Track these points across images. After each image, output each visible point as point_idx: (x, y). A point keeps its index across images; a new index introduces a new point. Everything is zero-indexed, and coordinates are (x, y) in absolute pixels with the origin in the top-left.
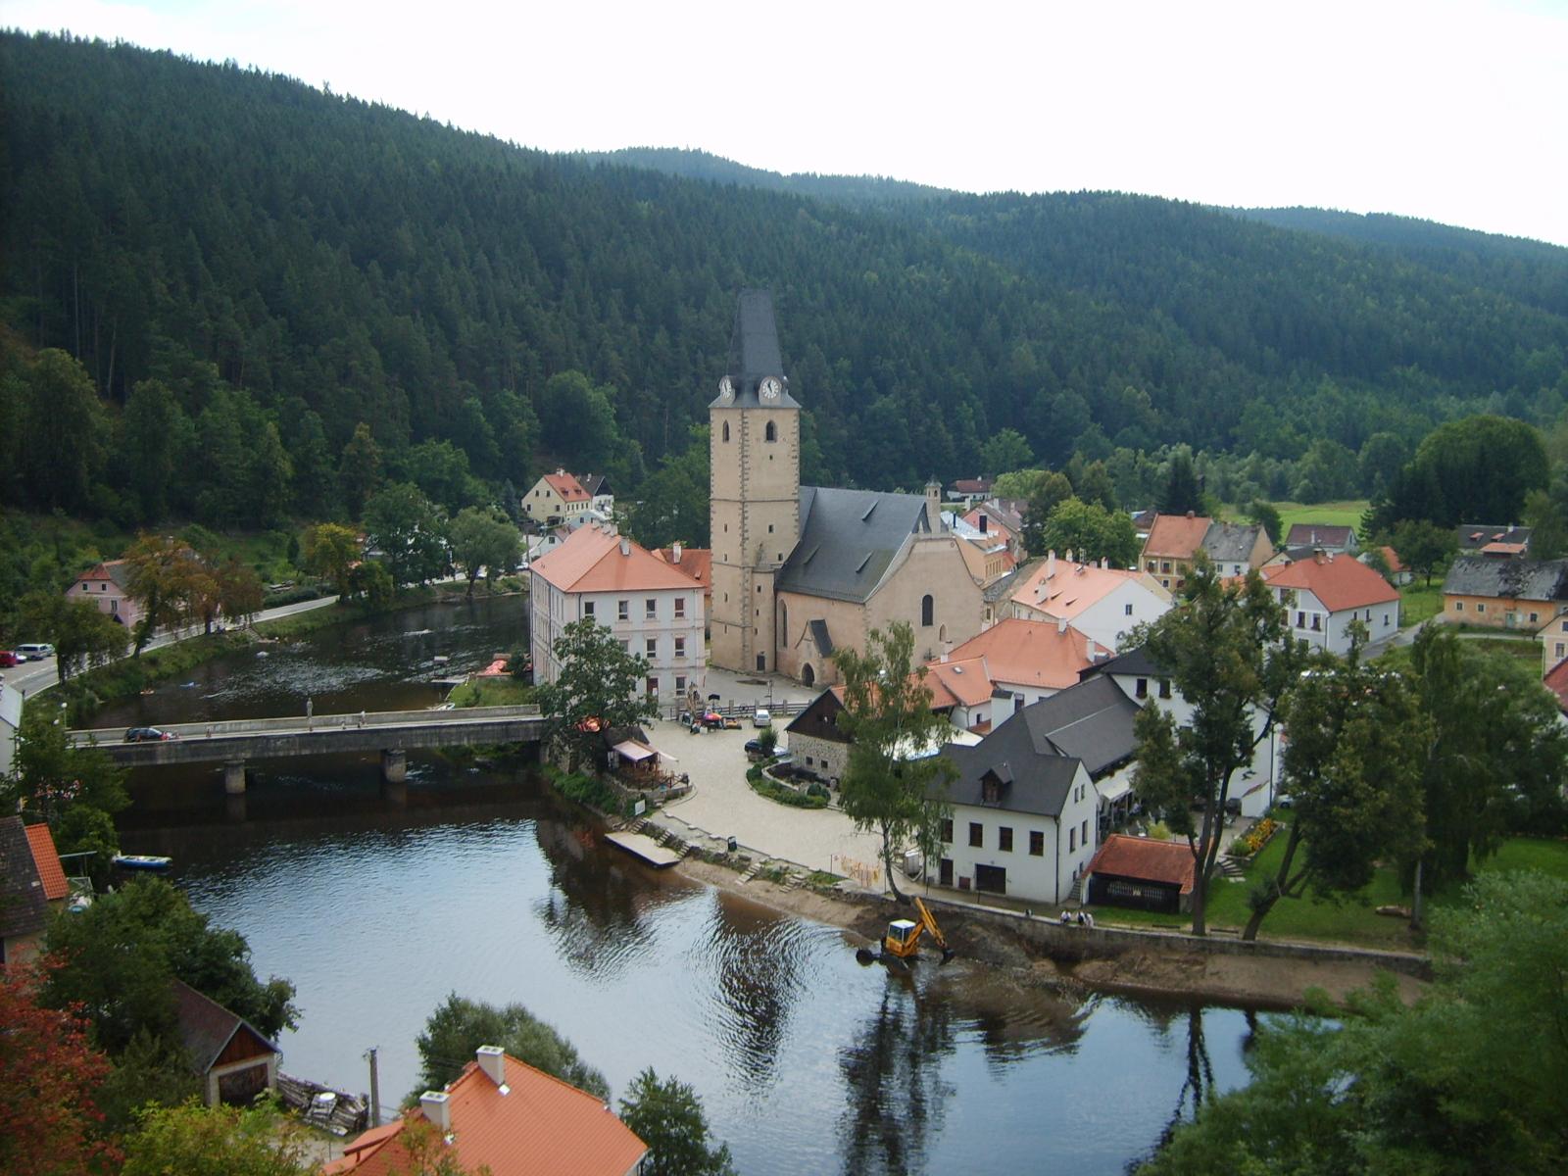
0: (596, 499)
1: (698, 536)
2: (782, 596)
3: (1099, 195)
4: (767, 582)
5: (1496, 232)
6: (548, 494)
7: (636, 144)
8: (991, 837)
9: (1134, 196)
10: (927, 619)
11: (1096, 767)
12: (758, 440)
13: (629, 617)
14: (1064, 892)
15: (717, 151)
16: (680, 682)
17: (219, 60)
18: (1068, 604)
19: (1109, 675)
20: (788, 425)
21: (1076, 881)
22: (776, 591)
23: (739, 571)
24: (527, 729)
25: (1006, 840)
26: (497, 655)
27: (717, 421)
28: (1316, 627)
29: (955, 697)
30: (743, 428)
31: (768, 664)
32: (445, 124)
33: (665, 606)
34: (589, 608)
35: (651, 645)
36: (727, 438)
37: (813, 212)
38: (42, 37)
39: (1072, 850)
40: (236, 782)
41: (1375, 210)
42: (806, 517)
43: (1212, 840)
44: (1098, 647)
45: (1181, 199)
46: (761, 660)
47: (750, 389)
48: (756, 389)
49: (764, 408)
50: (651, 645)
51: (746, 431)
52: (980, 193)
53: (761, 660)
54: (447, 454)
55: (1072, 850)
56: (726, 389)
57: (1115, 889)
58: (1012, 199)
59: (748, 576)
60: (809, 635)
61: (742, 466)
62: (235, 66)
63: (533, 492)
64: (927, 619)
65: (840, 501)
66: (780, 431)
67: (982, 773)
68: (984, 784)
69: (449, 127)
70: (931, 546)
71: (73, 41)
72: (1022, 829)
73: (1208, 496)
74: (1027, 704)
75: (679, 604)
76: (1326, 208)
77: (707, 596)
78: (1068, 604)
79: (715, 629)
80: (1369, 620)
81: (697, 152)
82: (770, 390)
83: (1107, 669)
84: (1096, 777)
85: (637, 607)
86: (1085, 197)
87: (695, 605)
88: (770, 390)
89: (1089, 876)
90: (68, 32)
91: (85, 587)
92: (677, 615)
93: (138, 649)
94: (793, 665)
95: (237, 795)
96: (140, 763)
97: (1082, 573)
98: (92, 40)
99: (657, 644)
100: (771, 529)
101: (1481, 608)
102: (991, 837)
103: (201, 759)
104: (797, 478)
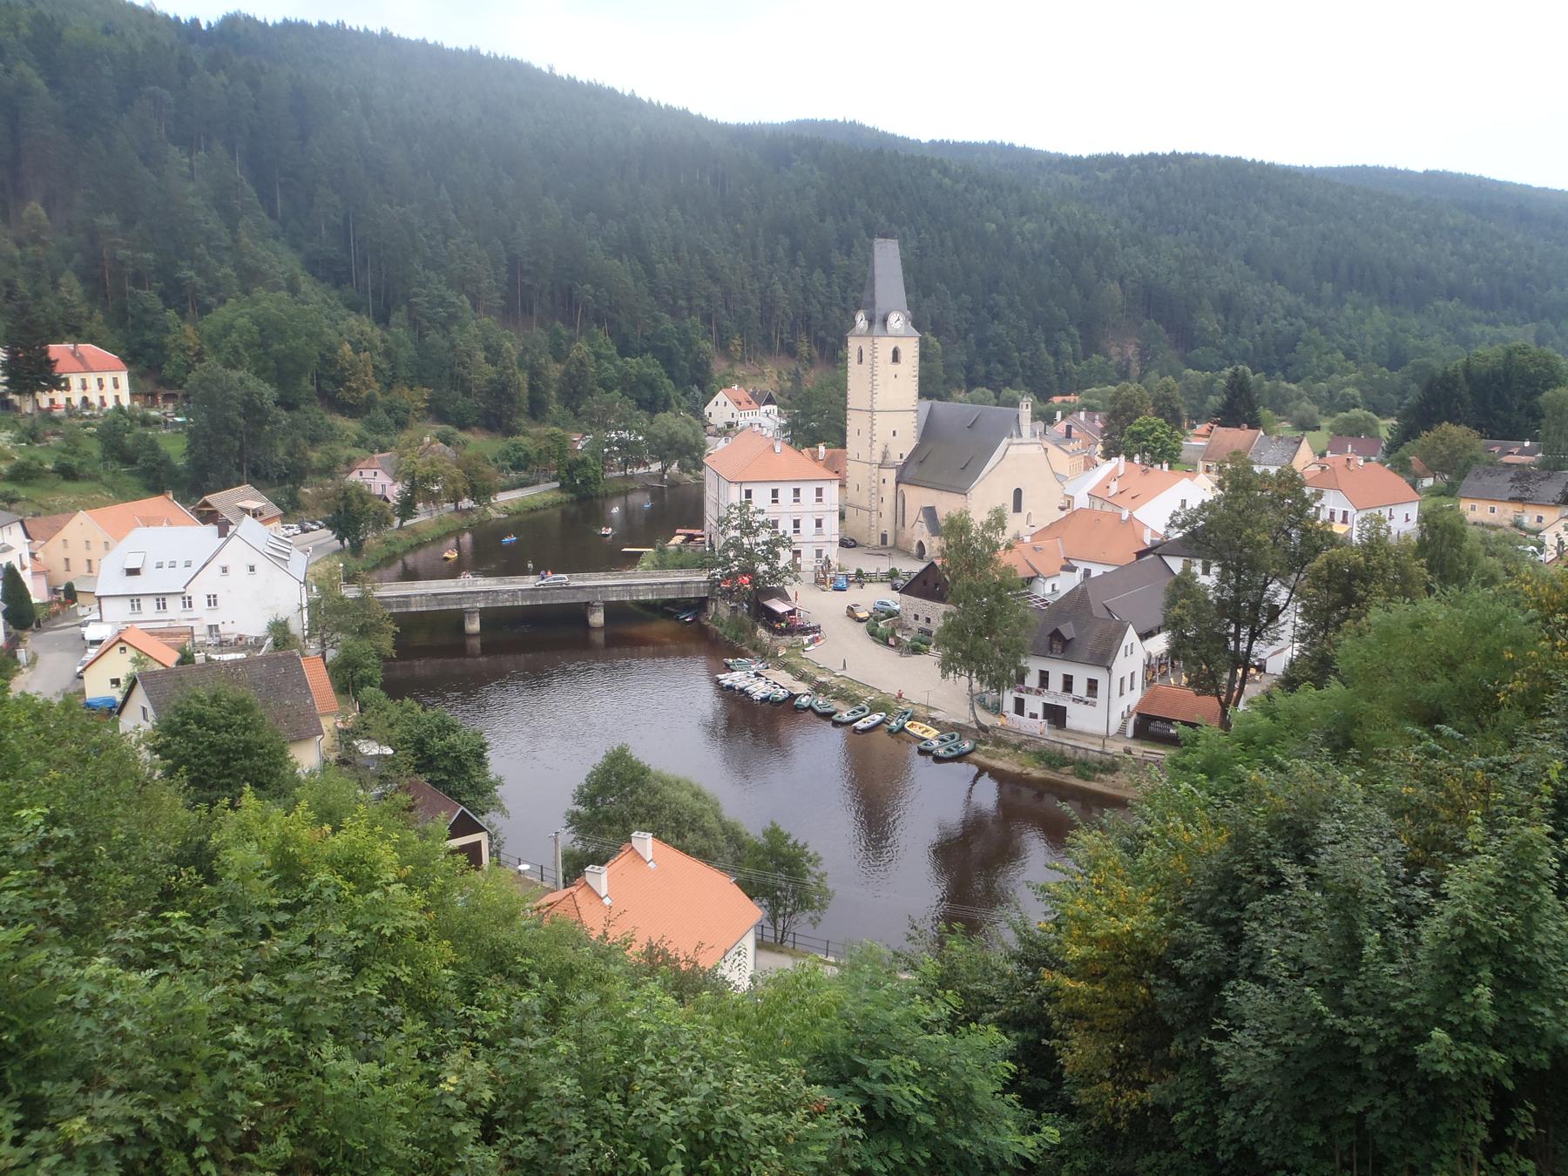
0: (764, 408)
1: (836, 434)
2: (902, 486)
3: (1189, 156)
4: (891, 475)
5: (1542, 185)
7: (802, 117)
8: (1056, 683)
9: (1217, 157)
10: (1017, 507)
11: (1145, 630)
12: (885, 361)
14: (1114, 729)
15: (869, 122)
16: (819, 553)
17: (465, 47)
19: (1160, 555)
20: (910, 349)
21: (1125, 719)
22: (897, 483)
24: (698, 588)
25: (1068, 683)
26: (678, 531)
27: (853, 344)
28: (1345, 521)
29: (1035, 570)
31: (890, 542)
33: (808, 492)
34: (748, 494)
35: (796, 524)
37: (945, 171)
38: (323, 27)
39: (1121, 694)
40: (474, 626)
41: (1432, 167)
42: (925, 418)
43: (1235, 694)
44: (1154, 533)
45: (1258, 160)
46: (884, 537)
47: (878, 322)
48: (885, 321)
50: (796, 524)
53: (884, 537)
54: (645, 366)
55: (1121, 694)
56: (861, 320)
57: (1155, 727)
58: (1112, 161)
59: (875, 470)
60: (921, 518)
62: (478, 51)
63: (713, 402)
64: (1017, 507)
65: (959, 408)
66: (903, 356)
67: (1050, 631)
68: (1051, 641)
72: (1081, 675)
73: (1265, 413)
74: (1093, 575)
75: (819, 492)
77: (842, 486)
79: (849, 512)
80: (1391, 518)
81: (853, 123)
83: (1158, 551)
84: (1144, 636)
85: (786, 493)
86: (1175, 157)
87: (832, 491)
88: (897, 321)
89: (1135, 716)
91: (361, 474)
92: (817, 500)
93: (401, 523)
94: (909, 542)
95: (474, 635)
96: (399, 610)
97: (1145, 472)
99: (801, 523)
101: (1493, 510)
102: (1056, 683)
103: (445, 608)
104: (916, 393)
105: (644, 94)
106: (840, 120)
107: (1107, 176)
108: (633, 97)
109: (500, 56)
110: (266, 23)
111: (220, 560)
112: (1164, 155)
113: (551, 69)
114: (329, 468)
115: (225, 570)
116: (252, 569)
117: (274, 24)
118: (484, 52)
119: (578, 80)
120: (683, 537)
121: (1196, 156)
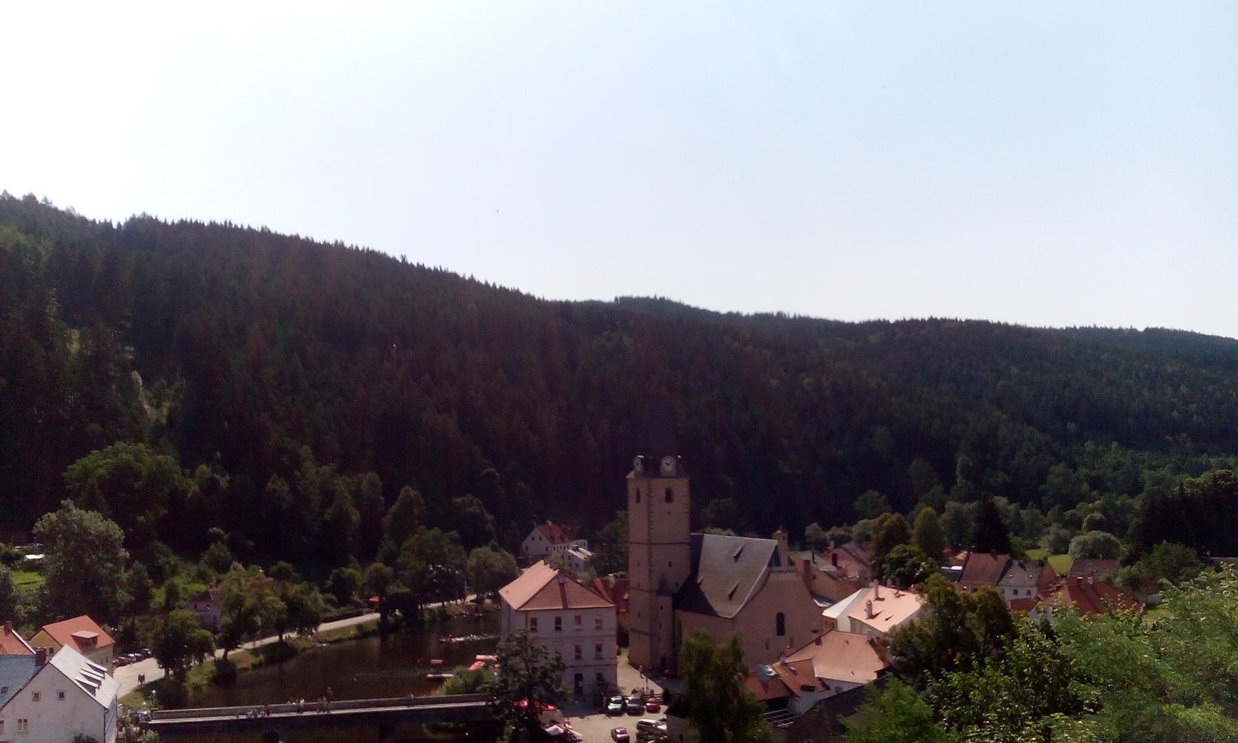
2: (679, 612)
3: (944, 321)
4: (666, 601)
6: (540, 539)
13: (563, 629)
18: (887, 619)
20: (681, 488)
23: (647, 595)
26: (479, 657)
30: (649, 492)
32: (461, 276)
36: (638, 500)
41: (1152, 326)
49: (664, 477)
51: (651, 494)
52: (857, 322)
61: (649, 520)
62: (342, 244)
69: (884, 320)
70: (783, 577)
71: (233, 227)
76: (1141, 329)
78: (887, 619)
81: (662, 300)
82: (668, 465)
90: (230, 223)
98: (245, 227)
100: (670, 565)
105: (481, 278)
106: (652, 296)
107: (873, 339)
108: (472, 280)
109: (360, 249)
110: (203, 224)
111: (35, 686)
112: (923, 320)
113: (404, 259)
114: (260, 596)
115: (37, 696)
116: (62, 695)
117: (173, 223)
118: (347, 245)
119: (426, 267)
120: (482, 664)
121: (951, 321)
